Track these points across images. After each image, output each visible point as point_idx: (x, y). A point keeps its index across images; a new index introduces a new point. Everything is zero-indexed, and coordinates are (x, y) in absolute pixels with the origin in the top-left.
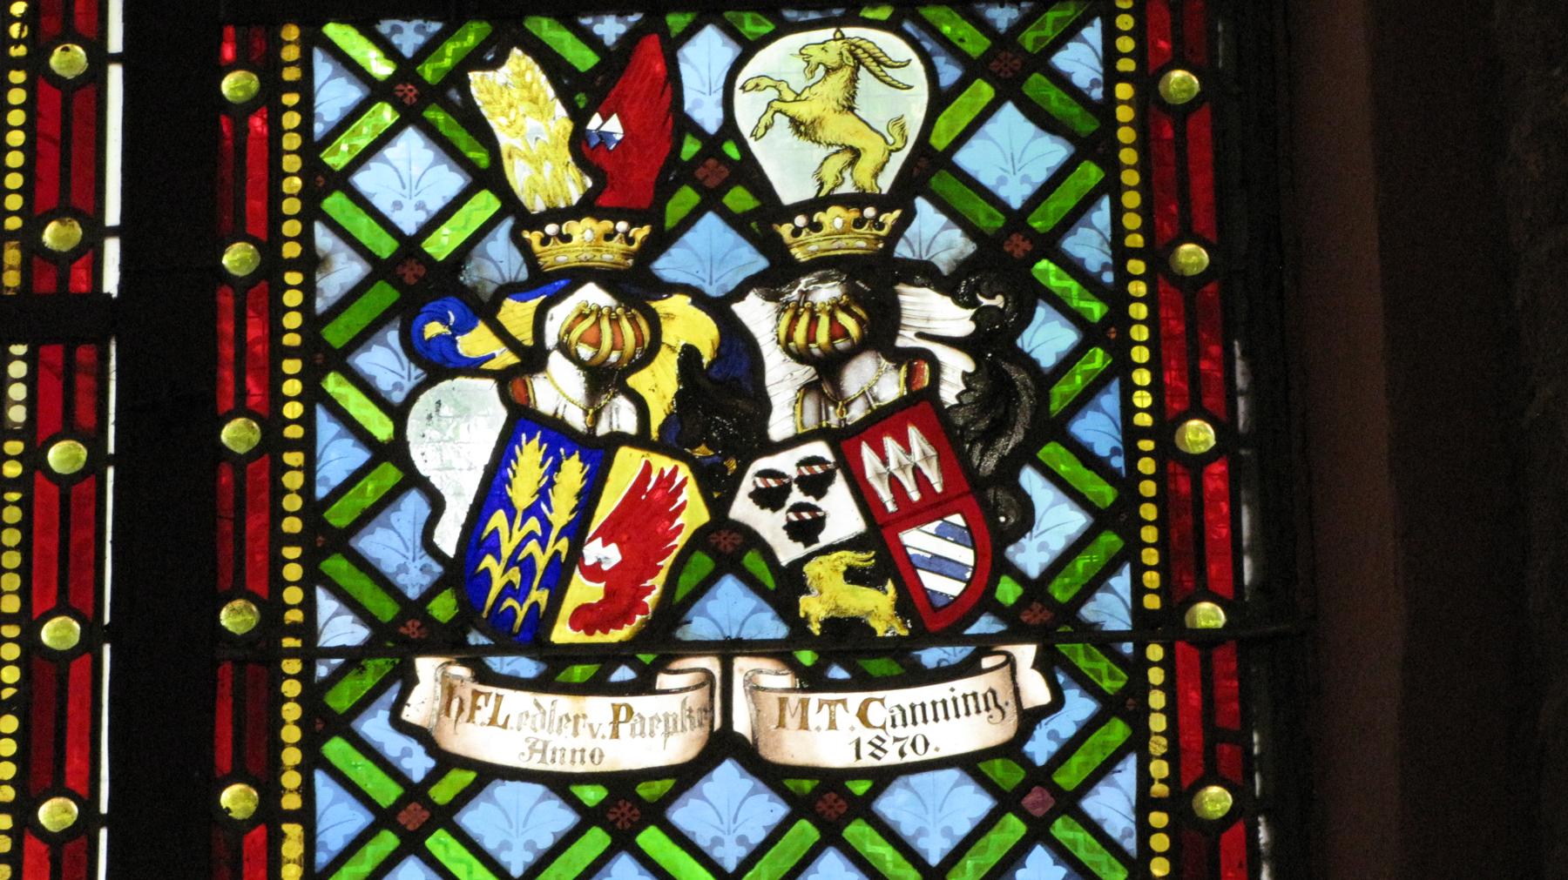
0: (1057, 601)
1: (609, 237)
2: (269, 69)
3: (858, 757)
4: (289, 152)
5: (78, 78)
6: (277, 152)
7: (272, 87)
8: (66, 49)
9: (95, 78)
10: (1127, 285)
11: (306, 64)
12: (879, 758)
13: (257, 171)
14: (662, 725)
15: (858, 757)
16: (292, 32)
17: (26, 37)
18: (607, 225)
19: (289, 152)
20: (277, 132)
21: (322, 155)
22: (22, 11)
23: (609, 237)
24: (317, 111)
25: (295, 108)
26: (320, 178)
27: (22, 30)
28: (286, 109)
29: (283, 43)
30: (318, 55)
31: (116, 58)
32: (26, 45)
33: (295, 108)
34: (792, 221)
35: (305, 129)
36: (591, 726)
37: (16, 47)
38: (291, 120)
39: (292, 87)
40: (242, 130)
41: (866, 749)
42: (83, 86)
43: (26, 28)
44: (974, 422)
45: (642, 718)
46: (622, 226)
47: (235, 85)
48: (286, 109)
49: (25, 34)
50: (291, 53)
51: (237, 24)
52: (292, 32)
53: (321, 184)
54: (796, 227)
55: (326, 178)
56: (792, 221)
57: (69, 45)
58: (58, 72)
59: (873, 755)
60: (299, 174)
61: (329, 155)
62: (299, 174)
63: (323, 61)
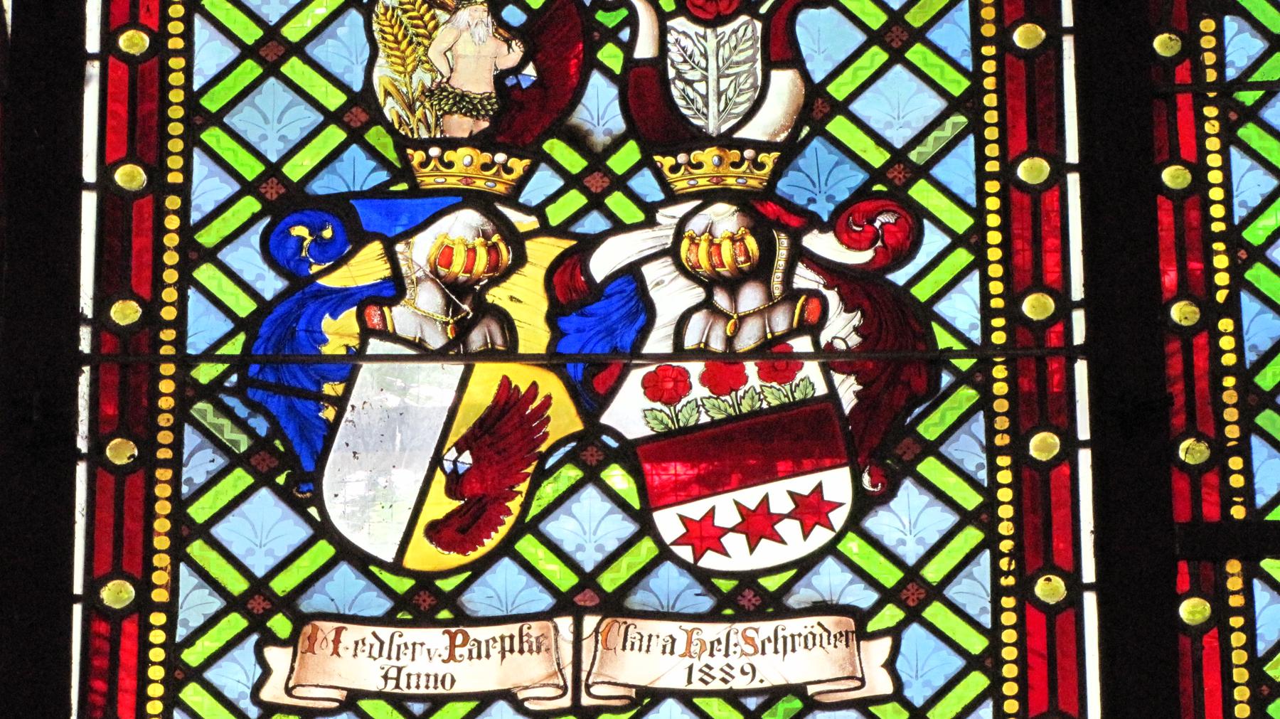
0: (167, 126)
1: (486, 167)
2: (1217, 596)
3: (689, 682)
4: (1238, 666)
5: (1058, 604)
6: (1227, 666)
7: (1221, 612)
8: (1049, 580)
9: (1073, 602)
10: (1218, 343)
11: (1248, 592)
12: (706, 683)
13: (1212, 682)
14: (498, 645)
15: (689, 682)
16: (1234, 566)
17: (1014, 569)
18: (486, 157)
19: (1238, 666)
20: (1227, 649)
21: (1265, 669)
22: (1010, 547)
23: (486, 167)
24: (1258, 632)
25: (1241, 629)
26: (1264, 688)
27: (1010, 564)
28: (1233, 630)
29: (1226, 576)
30: (1257, 584)
31: (1089, 587)
32: (1014, 576)
33: (1241, 629)
34: (675, 156)
35: (1250, 646)
36: (429, 651)
37: (1006, 578)
38: (1238, 639)
39: (1237, 612)
40: (1197, 649)
41: (696, 675)
42: (1065, 609)
43: (1013, 562)
44: (705, 277)
45: (479, 643)
46: (500, 157)
47: (1192, 610)
48: (1233, 630)
49: (1012, 567)
50: (1235, 584)
51: (1188, 560)
52: (1234, 566)
53: (1266, 693)
54: (677, 163)
55: (1270, 687)
56: (675, 156)
57: (1051, 577)
58: (1042, 598)
59: (702, 680)
60: (1247, 684)
61: (1271, 668)
62: (1247, 684)
63: (1262, 590)
